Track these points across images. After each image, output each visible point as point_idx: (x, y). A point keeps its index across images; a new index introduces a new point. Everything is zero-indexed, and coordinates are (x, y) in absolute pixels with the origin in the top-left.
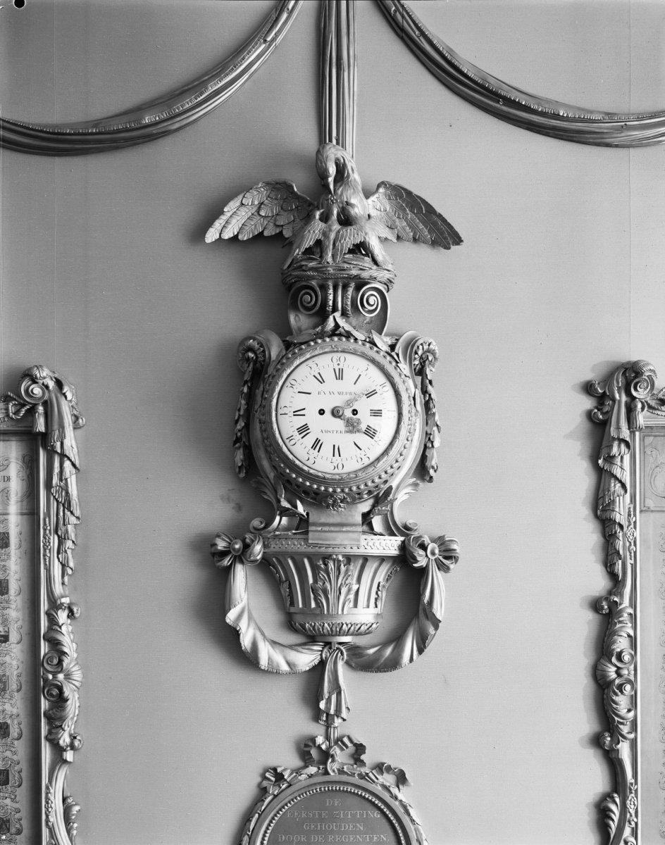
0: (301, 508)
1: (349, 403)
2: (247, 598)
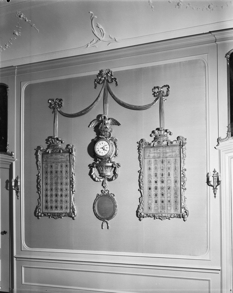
0: (100, 160)
1: (103, 147)
2: (95, 171)
